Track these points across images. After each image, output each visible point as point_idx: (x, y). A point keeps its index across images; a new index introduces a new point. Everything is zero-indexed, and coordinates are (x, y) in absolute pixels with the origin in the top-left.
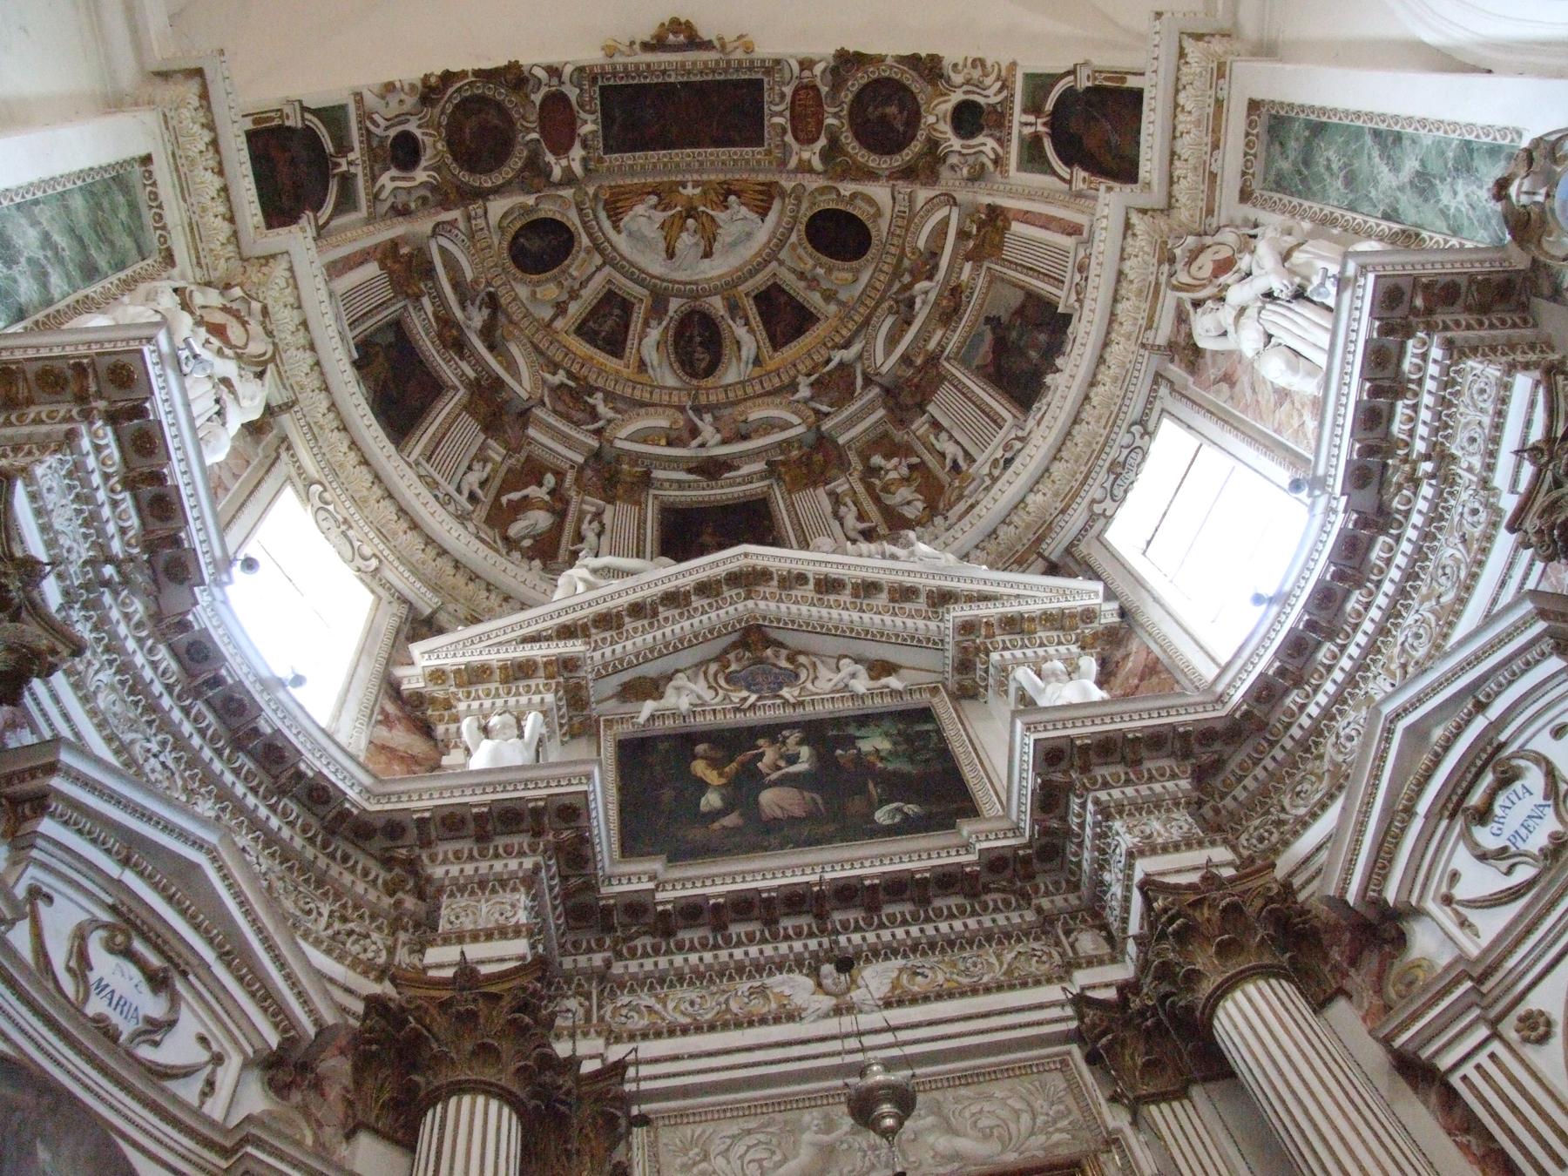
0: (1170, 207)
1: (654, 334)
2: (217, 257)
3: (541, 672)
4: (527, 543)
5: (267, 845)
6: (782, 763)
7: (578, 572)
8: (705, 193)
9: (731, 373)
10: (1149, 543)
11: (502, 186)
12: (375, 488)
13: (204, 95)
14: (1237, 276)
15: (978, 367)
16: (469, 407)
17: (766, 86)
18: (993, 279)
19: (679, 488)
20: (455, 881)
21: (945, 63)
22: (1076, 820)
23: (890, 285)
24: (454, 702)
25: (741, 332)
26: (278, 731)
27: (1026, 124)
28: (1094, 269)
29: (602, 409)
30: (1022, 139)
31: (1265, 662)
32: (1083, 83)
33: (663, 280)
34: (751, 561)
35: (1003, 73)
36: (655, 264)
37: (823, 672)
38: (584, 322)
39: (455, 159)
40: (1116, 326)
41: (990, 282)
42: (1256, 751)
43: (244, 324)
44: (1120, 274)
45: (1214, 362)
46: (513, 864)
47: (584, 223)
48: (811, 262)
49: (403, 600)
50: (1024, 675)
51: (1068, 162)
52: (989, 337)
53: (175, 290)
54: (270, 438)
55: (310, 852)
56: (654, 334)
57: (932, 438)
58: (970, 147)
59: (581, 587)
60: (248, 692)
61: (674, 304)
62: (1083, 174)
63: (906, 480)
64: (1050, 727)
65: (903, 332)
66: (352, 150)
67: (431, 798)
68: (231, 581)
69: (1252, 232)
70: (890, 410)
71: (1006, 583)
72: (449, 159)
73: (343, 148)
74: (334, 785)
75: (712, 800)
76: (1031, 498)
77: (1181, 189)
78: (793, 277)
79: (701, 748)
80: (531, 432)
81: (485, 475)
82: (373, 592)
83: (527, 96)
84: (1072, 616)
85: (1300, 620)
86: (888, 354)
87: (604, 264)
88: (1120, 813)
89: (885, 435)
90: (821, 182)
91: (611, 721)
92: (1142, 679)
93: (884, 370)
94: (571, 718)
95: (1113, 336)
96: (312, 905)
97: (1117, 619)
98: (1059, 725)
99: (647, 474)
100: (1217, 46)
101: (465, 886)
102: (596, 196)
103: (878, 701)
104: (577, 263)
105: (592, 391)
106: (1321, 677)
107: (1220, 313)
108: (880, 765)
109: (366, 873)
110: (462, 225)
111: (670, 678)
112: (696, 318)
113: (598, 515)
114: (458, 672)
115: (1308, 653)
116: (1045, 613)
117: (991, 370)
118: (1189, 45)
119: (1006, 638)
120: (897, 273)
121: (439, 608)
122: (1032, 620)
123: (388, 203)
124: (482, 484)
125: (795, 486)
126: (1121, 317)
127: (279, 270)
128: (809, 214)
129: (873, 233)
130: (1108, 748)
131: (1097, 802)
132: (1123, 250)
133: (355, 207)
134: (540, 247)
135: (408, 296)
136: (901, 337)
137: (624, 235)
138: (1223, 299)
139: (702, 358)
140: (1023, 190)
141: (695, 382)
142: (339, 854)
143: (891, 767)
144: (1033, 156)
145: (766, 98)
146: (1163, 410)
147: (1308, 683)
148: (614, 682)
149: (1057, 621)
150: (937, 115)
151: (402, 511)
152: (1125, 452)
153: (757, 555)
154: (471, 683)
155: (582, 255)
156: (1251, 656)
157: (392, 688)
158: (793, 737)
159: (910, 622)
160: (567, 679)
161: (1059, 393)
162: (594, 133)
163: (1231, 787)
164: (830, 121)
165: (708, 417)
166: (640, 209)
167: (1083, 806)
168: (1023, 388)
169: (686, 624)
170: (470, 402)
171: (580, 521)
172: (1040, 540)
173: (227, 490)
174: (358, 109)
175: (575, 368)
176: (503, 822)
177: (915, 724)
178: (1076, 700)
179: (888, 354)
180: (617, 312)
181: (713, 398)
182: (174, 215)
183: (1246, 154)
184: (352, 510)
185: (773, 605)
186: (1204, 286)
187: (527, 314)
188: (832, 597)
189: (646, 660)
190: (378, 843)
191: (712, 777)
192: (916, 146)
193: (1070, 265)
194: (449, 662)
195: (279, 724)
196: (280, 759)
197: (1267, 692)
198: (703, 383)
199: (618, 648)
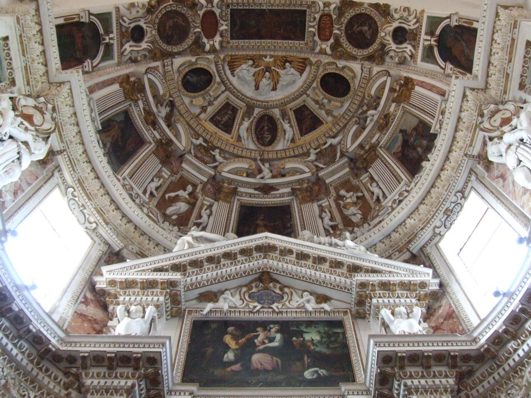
0: (486, 88)
1: (246, 124)
2: (38, 82)
3: (160, 286)
4: (174, 217)
5: (10, 362)
6: (266, 341)
7: (187, 238)
8: (275, 61)
9: (280, 145)
10: (461, 250)
11: (183, 51)
12: (101, 190)
13: (38, 10)
14: (510, 128)
15: (394, 153)
16: (155, 152)
17: (307, 13)
19: (249, 196)
20: (95, 387)
21: (391, 8)
22: (396, 392)
23: (356, 112)
24: (118, 296)
25: (287, 126)
26: (21, 310)
27: (426, 40)
28: (447, 115)
29: (218, 157)
30: (424, 47)
31: (498, 326)
32: (454, 23)
33: (252, 100)
35: (418, 15)
36: (249, 92)
37: (295, 297)
38: (214, 116)
39: (161, 38)
40: (455, 143)
41: (404, 113)
42: (491, 369)
43: (43, 113)
44: (459, 119)
45: (497, 167)
46: (123, 382)
47: (218, 71)
48: (322, 97)
49: (107, 243)
50: (385, 313)
51: (445, 60)
52: (400, 138)
53: (11, 98)
54: (50, 166)
55: (30, 367)
56: (246, 124)
57: (369, 184)
58: (401, 48)
59: (186, 246)
60: (9, 292)
61: (257, 111)
62: (451, 66)
63: (355, 204)
64: (387, 345)
65: (361, 132)
66: (112, 33)
67: (90, 346)
68: (6, 241)
69: (522, 106)
70: (352, 169)
71: (386, 264)
72: (158, 38)
73: (108, 31)
74: (46, 337)
75: (230, 356)
76: (408, 221)
77: (492, 80)
78: (313, 103)
79: (231, 329)
80: (184, 165)
81: (159, 184)
82: (92, 238)
83: (197, 12)
84: (415, 285)
85: (517, 307)
86: (353, 142)
87: (226, 90)
88: (417, 392)
89: (348, 181)
90: (330, 59)
91: (191, 311)
92: (445, 319)
93: (351, 150)
94: (172, 309)
95: (454, 148)
96: (26, 393)
97: (437, 288)
98: (391, 345)
99: (236, 189)
100: (515, 12)
101: (99, 391)
102: (224, 58)
103: (318, 315)
105: (214, 148)
106: (526, 336)
107: (500, 145)
108: (312, 347)
109: (56, 378)
110: (161, 69)
111: (222, 292)
113: (210, 207)
114: (121, 282)
115: (520, 323)
116: (401, 282)
117: (400, 154)
118: (501, 11)
119: (381, 292)
120: (360, 106)
121: (123, 248)
122: (394, 285)
123: (128, 57)
124: (157, 189)
125: (303, 201)
126: (458, 139)
127: (65, 89)
128: (323, 74)
129: (352, 85)
130: (414, 358)
131: (405, 385)
132: (461, 107)
133: (112, 58)
134: (197, 81)
135: (132, 100)
136: (360, 135)
137: (236, 78)
138: (502, 138)
139: (268, 137)
140: (425, 71)
141: (263, 148)
142: (44, 369)
143: (317, 349)
144: (429, 56)
145: (307, 19)
146: (472, 187)
147: (519, 338)
148: (196, 293)
149: (406, 286)
150: (386, 32)
151: (113, 201)
152: (453, 205)
153: (271, 238)
154: (127, 288)
155: (216, 85)
156: (492, 321)
157: (92, 286)
158: (274, 328)
159: (338, 278)
160: (171, 291)
161: (426, 172)
162: (226, 30)
163: (476, 385)
164: (336, 31)
165: (267, 165)
166: (244, 66)
167: (399, 385)
168: (413, 167)
169: (233, 268)
170: (156, 149)
171: (201, 208)
172: (410, 242)
173: (23, 191)
174: (117, 14)
175: (207, 138)
176: (122, 362)
177: (333, 328)
178: (407, 331)
179: (353, 142)
180: (230, 112)
181: (270, 156)
182: (17, 62)
183: (523, 66)
184: (87, 200)
185: (275, 263)
186: (495, 131)
187: (188, 111)
188: (303, 262)
189: (212, 284)
190: (64, 364)
191: (233, 344)
192: (375, 46)
193: (438, 112)
194: (120, 277)
195: (22, 307)
196: (22, 323)
197: (498, 340)
199: (199, 277)
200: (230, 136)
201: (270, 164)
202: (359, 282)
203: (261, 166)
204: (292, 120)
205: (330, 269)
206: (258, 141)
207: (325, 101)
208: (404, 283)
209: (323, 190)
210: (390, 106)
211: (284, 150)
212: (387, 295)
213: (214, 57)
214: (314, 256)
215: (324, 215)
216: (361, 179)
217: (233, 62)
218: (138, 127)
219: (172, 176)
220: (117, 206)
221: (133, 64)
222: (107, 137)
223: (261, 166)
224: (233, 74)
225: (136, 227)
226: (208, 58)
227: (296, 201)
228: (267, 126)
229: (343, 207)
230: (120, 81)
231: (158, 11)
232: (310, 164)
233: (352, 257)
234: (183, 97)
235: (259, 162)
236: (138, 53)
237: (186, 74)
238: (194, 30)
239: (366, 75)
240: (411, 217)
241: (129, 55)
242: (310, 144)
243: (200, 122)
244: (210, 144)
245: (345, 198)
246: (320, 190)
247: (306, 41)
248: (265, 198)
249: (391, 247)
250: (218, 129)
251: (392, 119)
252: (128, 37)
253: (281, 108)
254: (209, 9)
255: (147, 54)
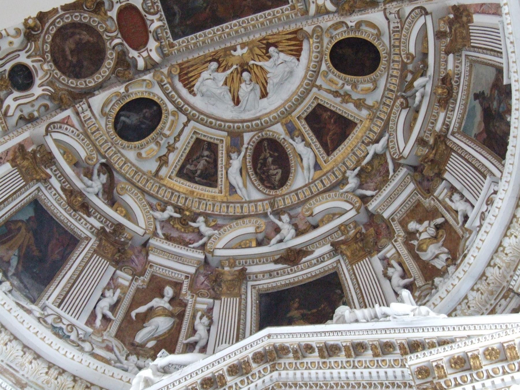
1: (236, 163)
8: (251, 50)
9: (299, 179)
15: (476, 136)
16: (98, 251)
18: (473, 63)
25: (300, 147)
29: (204, 228)
33: (234, 122)
34: (272, 341)
36: (226, 111)
39: (64, 73)
41: (471, 66)
47: (167, 95)
56: (236, 163)
61: (247, 137)
63: (435, 238)
70: (419, 183)
76: (507, 242)
78: (331, 96)
80: (152, 257)
81: (115, 299)
83: (106, 14)
86: (406, 142)
89: (419, 204)
90: (337, 19)
93: (406, 153)
99: (244, 270)
104: (168, 125)
110: (74, 120)
112: (266, 143)
117: (485, 135)
119: (458, 376)
125: (354, 259)
128: (330, 47)
129: (380, 48)
135: (38, 181)
137: (199, 96)
139: (277, 173)
141: (273, 192)
151: (26, 348)
153: (277, 335)
155: (171, 118)
159: (390, 371)
166: (205, 75)
171: (194, 317)
179: (406, 142)
180: (206, 153)
181: (288, 202)
188: (332, 360)
198: (279, 192)
200: (217, 190)
201: (289, 215)
202: (414, 368)
203: (277, 221)
204: (306, 136)
205: (376, 359)
206: (263, 184)
207: (348, 88)
208: (493, 349)
209: (384, 232)
210: (446, 61)
211: (306, 186)
212: (469, 378)
213: (154, 76)
214: (344, 344)
215: (390, 271)
216: (435, 194)
217: (186, 74)
218: (61, 221)
219: (136, 280)
220: (35, 353)
221: (29, 125)
222: (10, 248)
223: (277, 221)
224: (192, 92)
225: (75, 379)
226: (144, 80)
227: (345, 261)
228: (271, 156)
229: (418, 250)
230: (10, 157)
231: (44, 33)
232: (350, 196)
233: (404, 329)
234: (122, 151)
235: (272, 217)
236: (33, 106)
237: (118, 116)
238: (110, 43)
239: (396, 25)
240: (508, 234)
241: (18, 114)
242: (344, 163)
243: (162, 182)
244: (187, 213)
245: (418, 235)
246: (378, 234)
247: (291, 3)
248: (295, 272)
249: (492, 293)
250: (195, 185)
251: (456, 82)
252: (7, 87)
253: (284, 121)
254: (124, 4)
255: (48, 103)
